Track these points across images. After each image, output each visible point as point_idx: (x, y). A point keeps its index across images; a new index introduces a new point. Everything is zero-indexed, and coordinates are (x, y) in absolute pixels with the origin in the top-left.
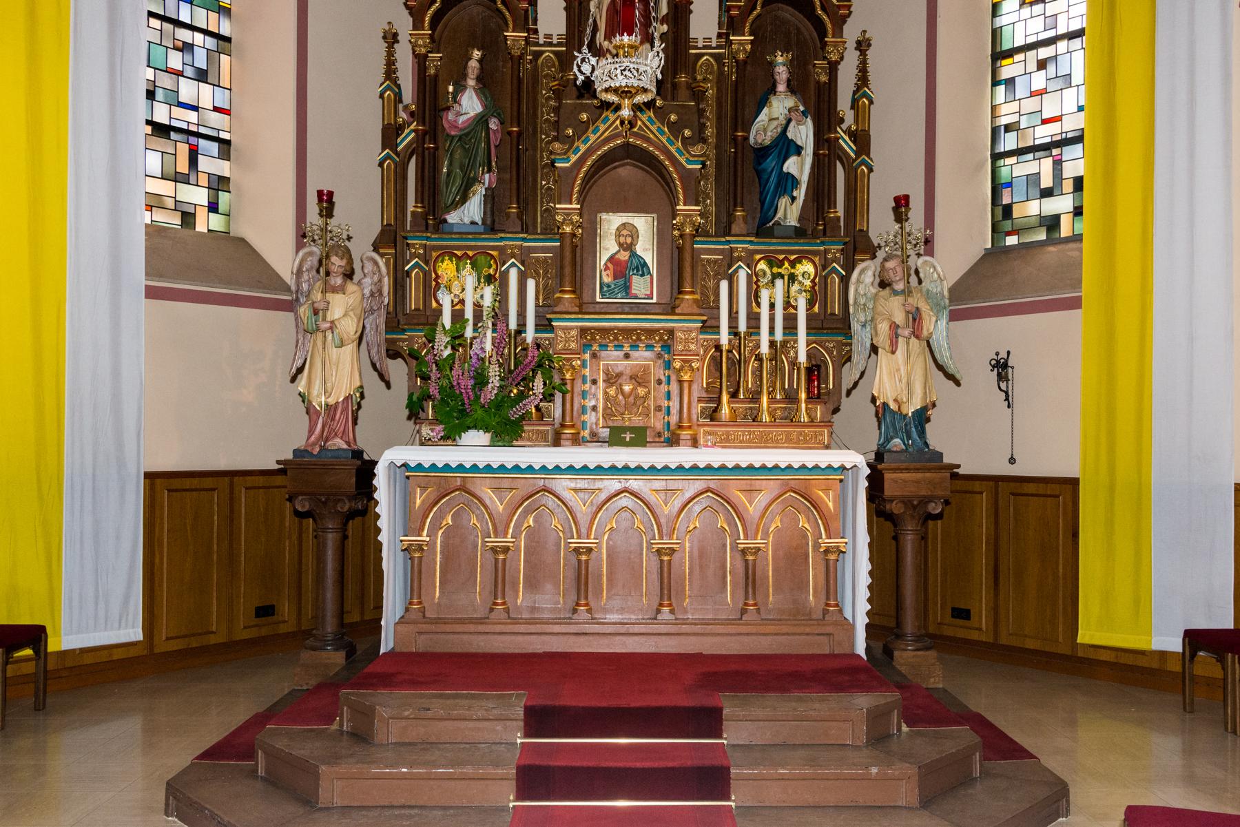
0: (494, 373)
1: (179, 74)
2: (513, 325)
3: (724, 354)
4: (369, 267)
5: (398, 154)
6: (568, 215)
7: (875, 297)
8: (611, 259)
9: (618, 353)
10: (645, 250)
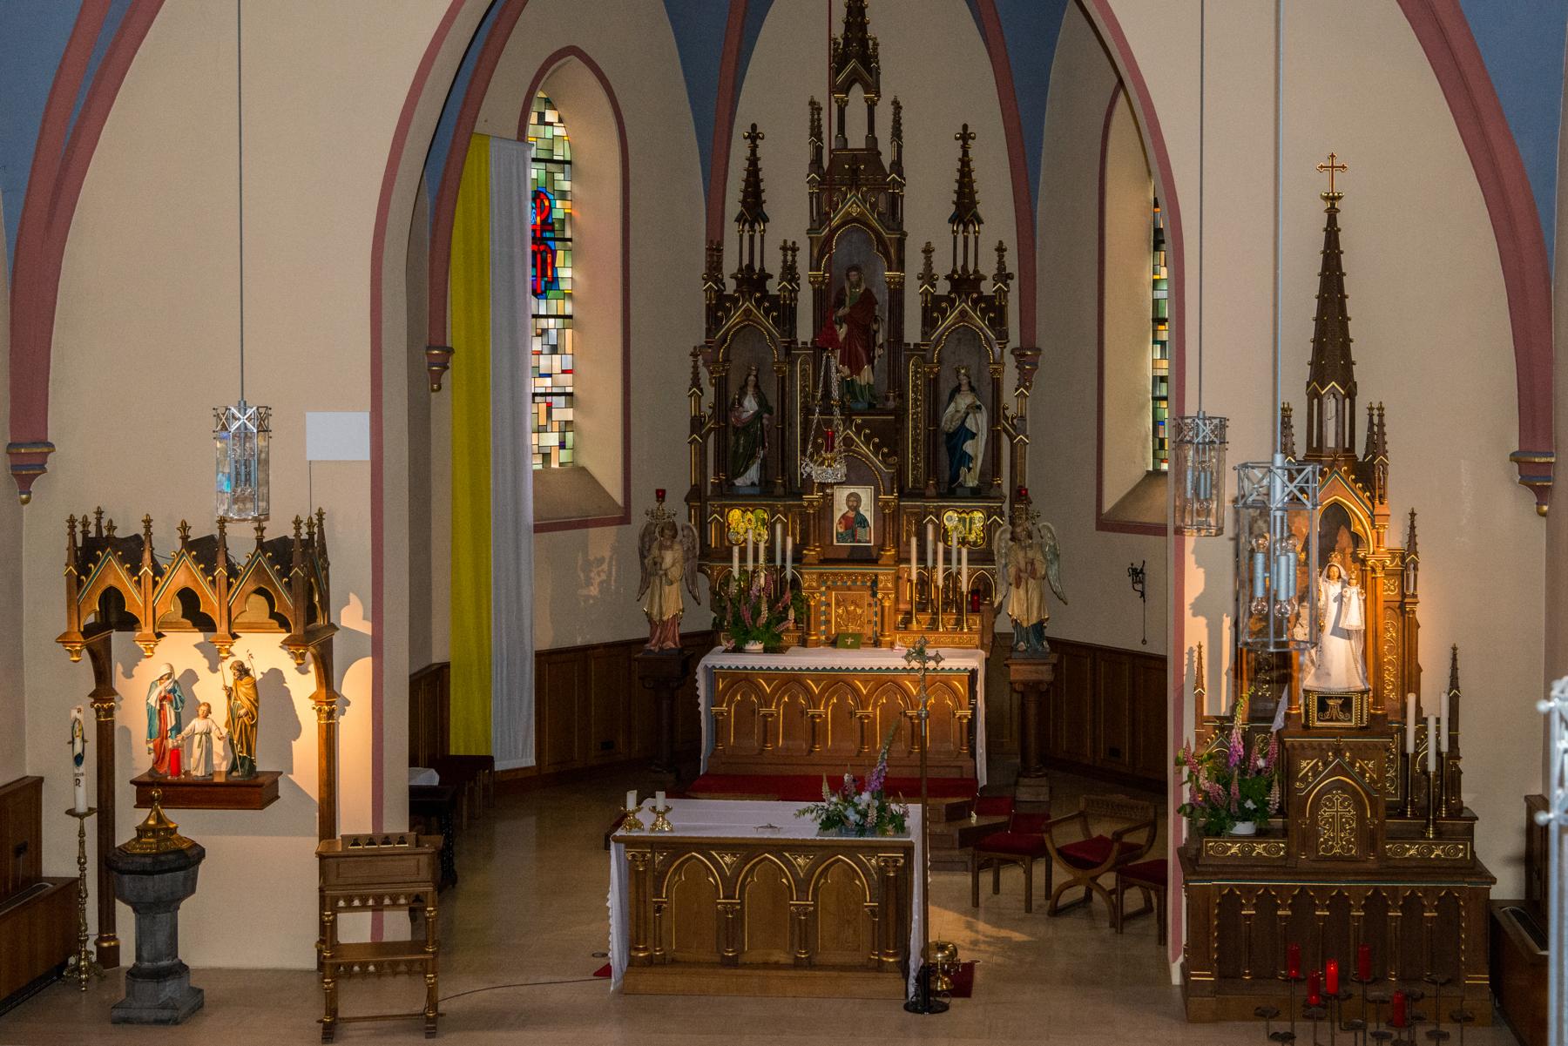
2: (778, 563)
8: (844, 516)
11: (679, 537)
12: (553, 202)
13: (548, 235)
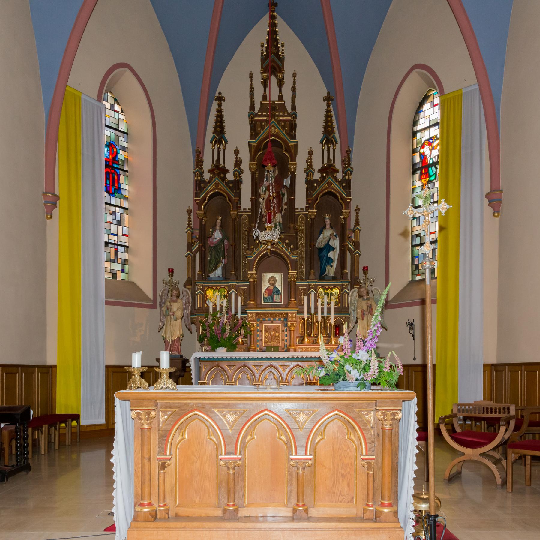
0: (228, 328)
1: (111, 223)
2: (233, 312)
3: (306, 321)
4: (185, 293)
5: (192, 253)
6: (252, 275)
7: (358, 301)
8: (267, 289)
9: (269, 321)
10: (279, 286)
11: (181, 296)
12: (118, 150)
13: (116, 166)
